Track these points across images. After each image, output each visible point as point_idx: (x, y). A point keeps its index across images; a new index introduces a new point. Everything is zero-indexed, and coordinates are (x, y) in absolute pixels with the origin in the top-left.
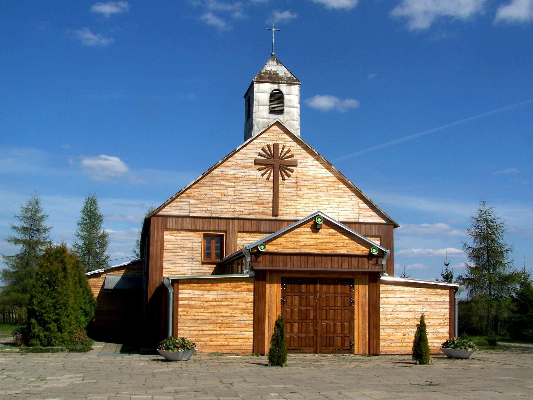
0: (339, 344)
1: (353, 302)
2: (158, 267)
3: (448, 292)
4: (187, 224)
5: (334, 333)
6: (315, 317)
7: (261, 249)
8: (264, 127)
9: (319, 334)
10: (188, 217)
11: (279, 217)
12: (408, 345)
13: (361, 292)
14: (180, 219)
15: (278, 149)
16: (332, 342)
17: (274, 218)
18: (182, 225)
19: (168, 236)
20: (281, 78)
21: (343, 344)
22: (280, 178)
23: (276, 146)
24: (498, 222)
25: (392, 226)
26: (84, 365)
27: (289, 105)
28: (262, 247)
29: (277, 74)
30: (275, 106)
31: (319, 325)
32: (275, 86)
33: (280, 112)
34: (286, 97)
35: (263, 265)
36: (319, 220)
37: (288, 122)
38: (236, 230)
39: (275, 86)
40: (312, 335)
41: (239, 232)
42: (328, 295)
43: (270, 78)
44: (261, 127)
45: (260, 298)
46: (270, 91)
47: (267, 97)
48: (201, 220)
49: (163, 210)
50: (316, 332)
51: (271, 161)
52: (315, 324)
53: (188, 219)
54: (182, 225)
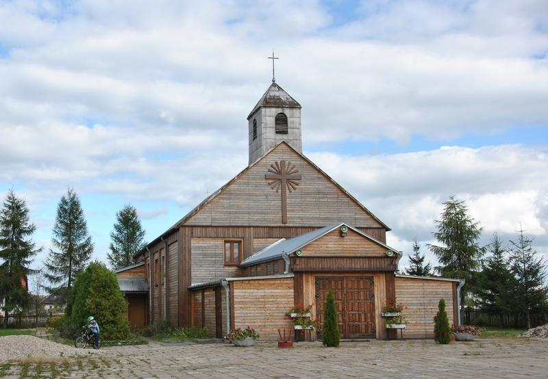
0: (364, 331)
1: (374, 296)
2: (187, 269)
3: (451, 284)
4: (211, 231)
5: (359, 322)
6: (343, 309)
7: (299, 254)
8: (271, 147)
9: (347, 322)
10: (211, 226)
11: (287, 225)
12: (431, 329)
13: (380, 288)
14: (204, 229)
15: (284, 165)
16: (358, 329)
17: (283, 225)
18: (206, 234)
19: (195, 243)
20: (284, 103)
21: (366, 331)
22: (288, 191)
23: (283, 163)
24: (478, 227)
25: (384, 230)
26: (120, 358)
27: (292, 126)
28: (299, 252)
29: (280, 99)
30: (281, 128)
31: (347, 316)
32: (280, 111)
33: (285, 132)
34: (289, 120)
35: (300, 265)
36: (344, 229)
37: (291, 142)
38: (252, 236)
39: (280, 111)
40: (341, 324)
41: (254, 238)
42: (352, 290)
43: (275, 103)
44: (268, 146)
45: (298, 295)
46: (275, 115)
47: (273, 120)
48: (222, 229)
49: (189, 221)
50: (344, 321)
51: (278, 176)
52: (343, 315)
53: (210, 228)
54: (206, 234)
